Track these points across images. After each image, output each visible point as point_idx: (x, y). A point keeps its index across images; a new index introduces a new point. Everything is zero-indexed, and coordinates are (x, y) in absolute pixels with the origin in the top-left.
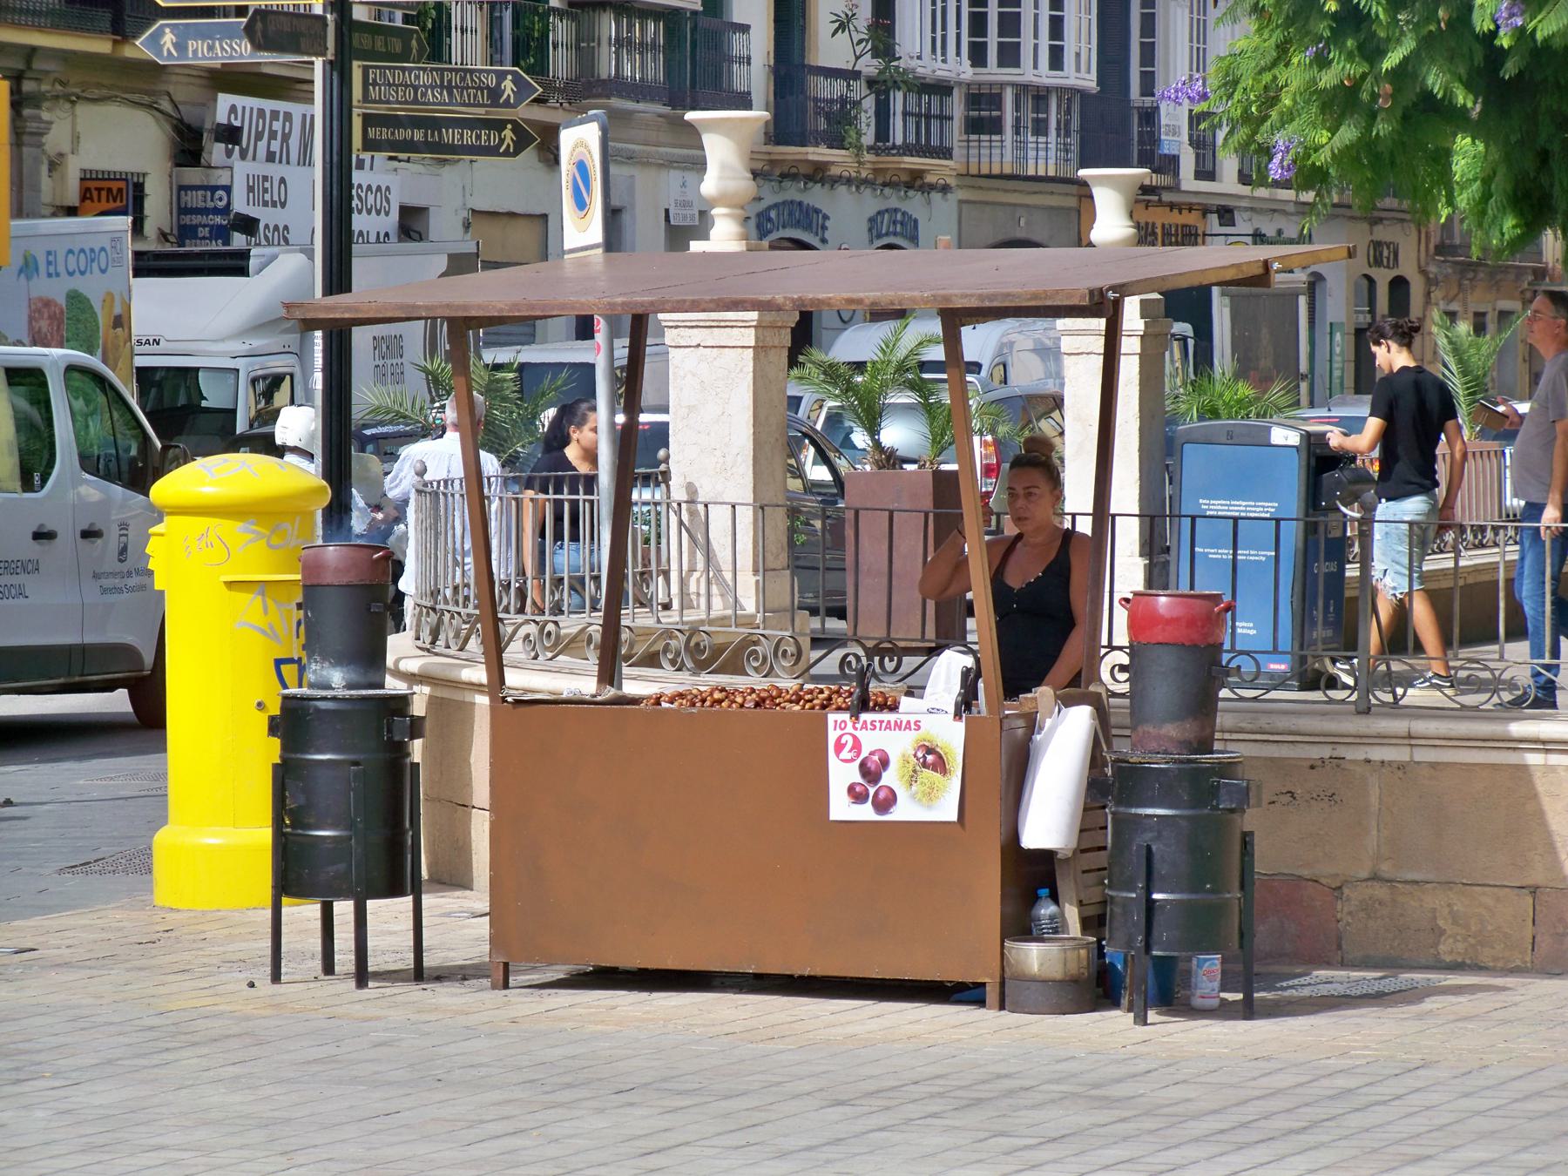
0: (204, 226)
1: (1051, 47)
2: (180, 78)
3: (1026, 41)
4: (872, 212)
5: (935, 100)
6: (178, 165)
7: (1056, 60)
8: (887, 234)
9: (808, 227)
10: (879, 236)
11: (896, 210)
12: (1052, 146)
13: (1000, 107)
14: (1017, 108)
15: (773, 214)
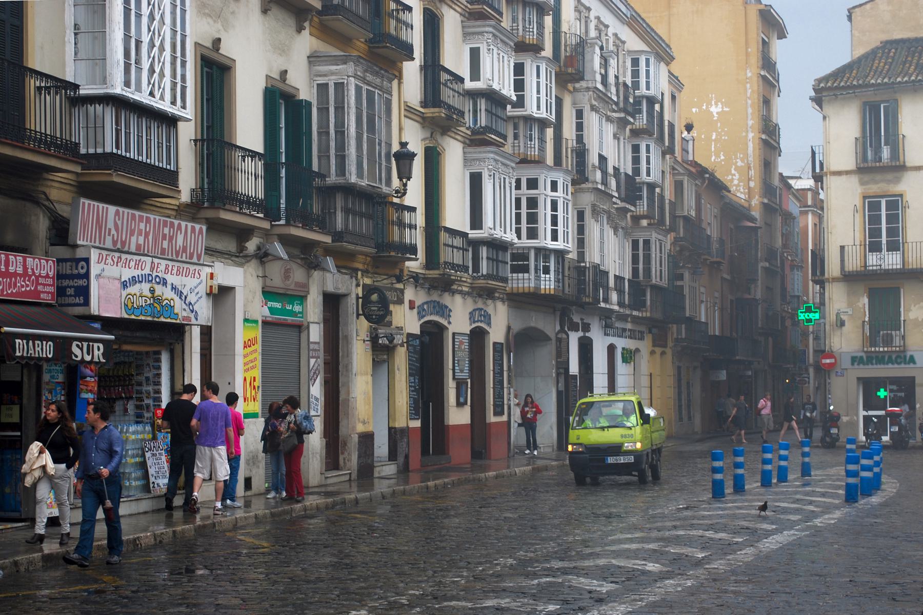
0: (71, 287)
1: (557, 226)
2: (56, 185)
3: (541, 226)
4: (471, 310)
5: (500, 253)
6: (52, 245)
7: (555, 238)
8: (478, 321)
9: (442, 316)
10: (474, 322)
11: (481, 309)
12: (552, 279)
13: (527, 259)
14: (536, 260)
15: (425, 307)
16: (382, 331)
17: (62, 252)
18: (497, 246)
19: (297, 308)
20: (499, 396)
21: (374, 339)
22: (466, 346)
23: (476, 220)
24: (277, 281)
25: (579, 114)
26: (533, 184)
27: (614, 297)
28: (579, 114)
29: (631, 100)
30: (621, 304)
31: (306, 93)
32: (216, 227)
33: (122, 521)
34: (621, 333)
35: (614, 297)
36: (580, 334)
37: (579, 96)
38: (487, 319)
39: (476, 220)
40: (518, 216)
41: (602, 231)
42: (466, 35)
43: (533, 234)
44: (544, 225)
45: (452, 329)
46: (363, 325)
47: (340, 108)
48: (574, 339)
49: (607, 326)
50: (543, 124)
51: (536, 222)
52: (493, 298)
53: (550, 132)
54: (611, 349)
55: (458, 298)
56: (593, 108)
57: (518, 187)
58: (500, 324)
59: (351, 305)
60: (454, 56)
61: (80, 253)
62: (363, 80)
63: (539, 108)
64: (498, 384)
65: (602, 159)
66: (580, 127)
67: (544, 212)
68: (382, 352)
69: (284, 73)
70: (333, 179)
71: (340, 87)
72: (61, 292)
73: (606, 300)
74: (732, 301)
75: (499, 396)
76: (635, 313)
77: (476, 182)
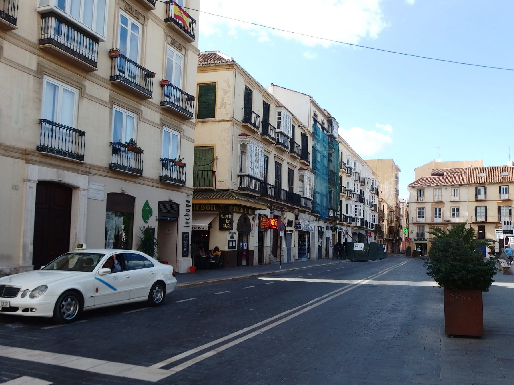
18: (350, 217)
23: (347, 213)
26: (356, 206)
32: (314, 216)
33: (440, 191)
39: (347, 213)
43: (356, 215)
44: (358, 214)
51: (278, 122)
67: (358, 211)
74: (185, 234)
77: (347, 206)
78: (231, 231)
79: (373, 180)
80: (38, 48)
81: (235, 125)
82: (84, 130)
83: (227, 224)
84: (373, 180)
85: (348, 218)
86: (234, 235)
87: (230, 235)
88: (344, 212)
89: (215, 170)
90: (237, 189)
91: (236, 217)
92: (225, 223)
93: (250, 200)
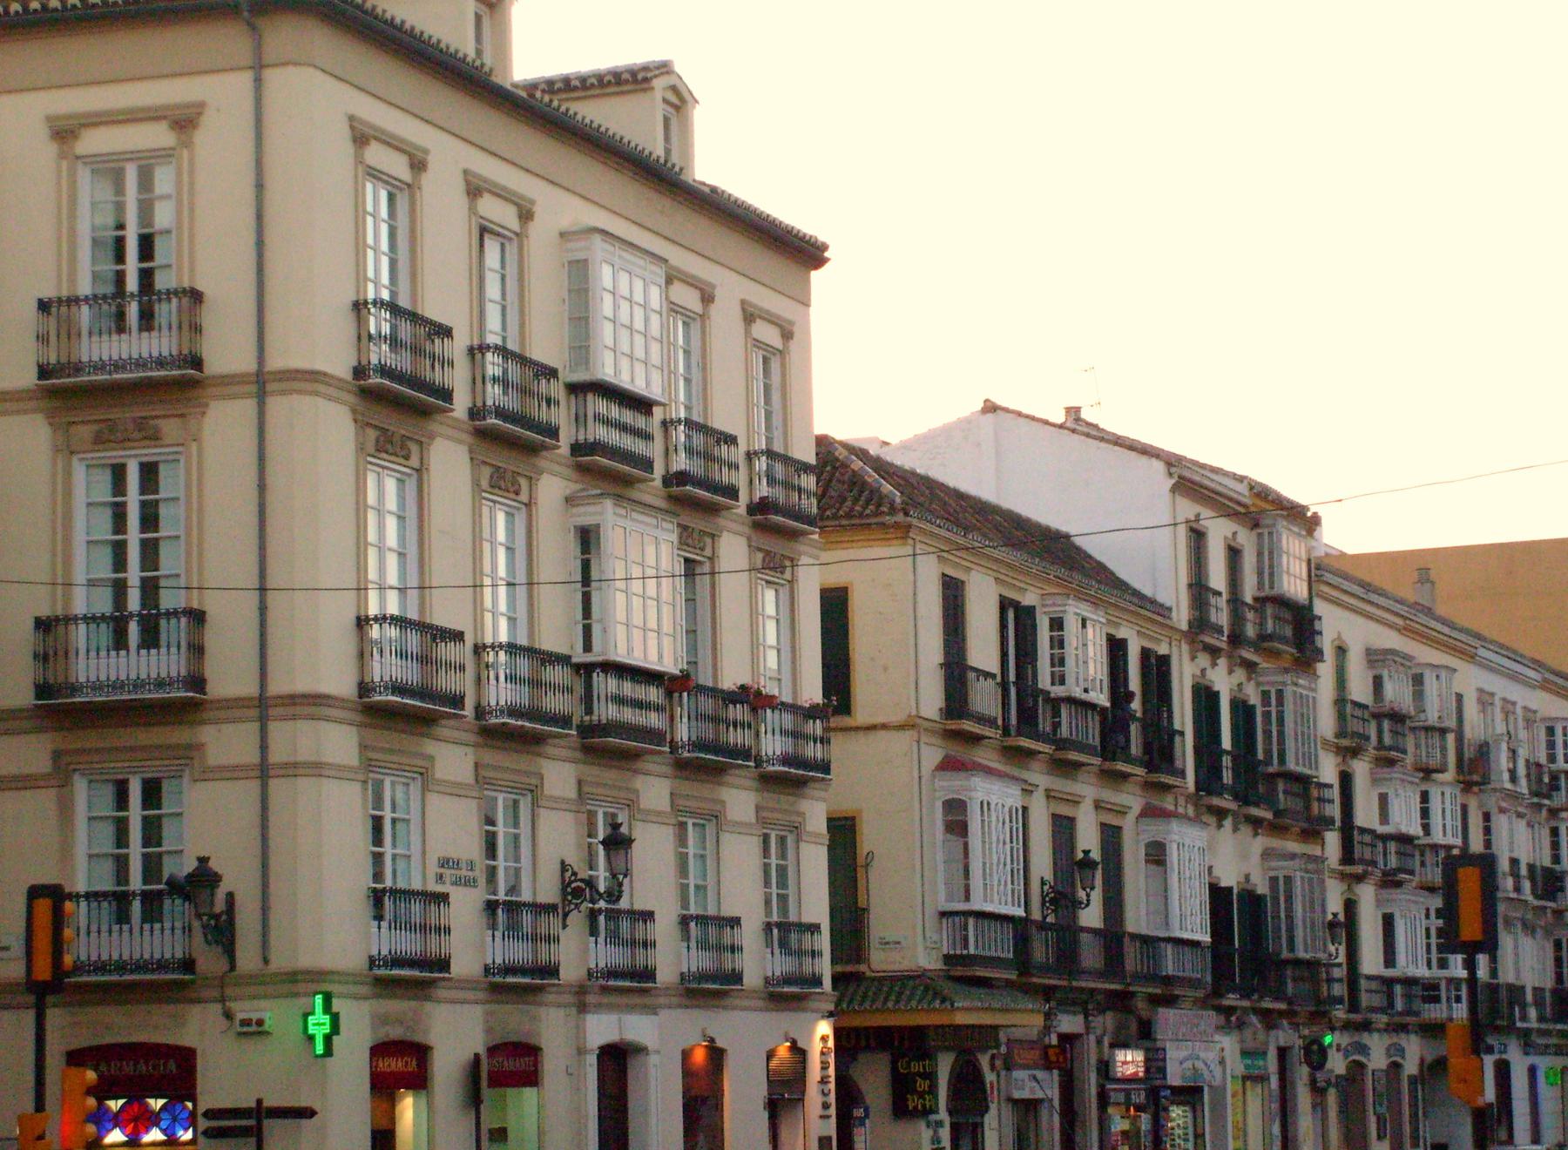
16: (1319, 1076)
17: (1148, 1044)
18: (1409, 982)
19: (1261, 1063)
20: (1415, 1130)
21: (1313, 1082)
22: (1383, 1081)
24: (1250, 1045)
25: (1487, 817)
27: (1533, 1013)
28: (1487, 817)
29: (1546, 780)
30: (1541, 1019)
31: (1262, 889)
32: (1219, 1009)
34: (1544, 1051)
35: (1533, 1013)
36: (1497, 1056)
37: (1484, 797)
38: (1401, 1051)
40: (1429, 945)
41: (1516, 941)
42: (1375, 781)
45: (1371, 1066)
46: (1305, 1070)
47: (1289, 898)
48: (1489, 1061)
49: (1526, 1045)
50: (1443, 731)
52: (1408, 1032)
53: (1451, 738)
54: (1532, 1071)
55: (1376, 1035)
56: (1502, 811)
57: (1427, 916)
58: (1414, 1052)
59: (1297, 1054)
60: (1365, 815)
61: (1159, 1044)
62: (1307, 871)
63: (1445, 834)
64: (1414, 1116)
65: (1514, 862)
66: (1487, 831)
68: (1318, 1091)
69: (1247, 877)
70: (1285, 954)
71: (1288, 879)
72: (1147, 1070)
73: (1524, 1018)
75: (1415, 1130)
76: (1559, 1027)
77: (1388, 922)
78: (933, 1117)
79: (1551, 731)
80: (578, 745)
81: (924, 739)
82: (648, 907)
83: (921, 1095)
84: (1551, 731)
85: (1398, 989)
86: (941, 1130)
87: (931, 1132)
88: (1371, 962)
89: (862, 903)
90: (939, 965)
91: (944, 1066)
92: (914, 1091)
93: (996, 1005)
